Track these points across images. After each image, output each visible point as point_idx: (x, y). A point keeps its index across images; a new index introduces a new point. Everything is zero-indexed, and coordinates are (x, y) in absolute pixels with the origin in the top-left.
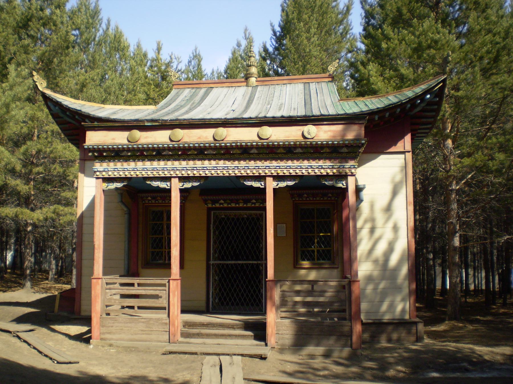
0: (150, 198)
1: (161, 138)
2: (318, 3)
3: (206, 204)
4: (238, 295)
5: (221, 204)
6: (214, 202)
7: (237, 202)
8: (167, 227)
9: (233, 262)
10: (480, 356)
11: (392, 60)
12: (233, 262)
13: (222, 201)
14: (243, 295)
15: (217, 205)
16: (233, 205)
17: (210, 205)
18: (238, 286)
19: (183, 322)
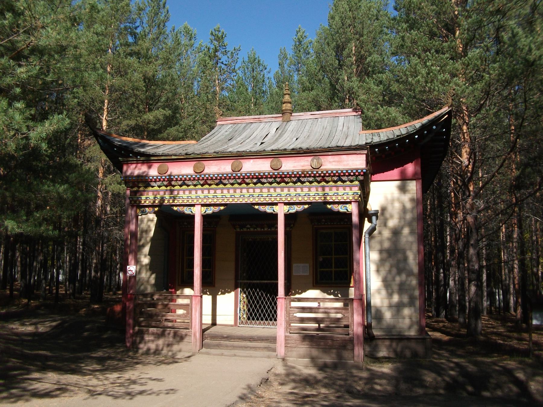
0: (185, 223)
1: (236, 343)
2: (363, 4)
3: (235, 228)
4: (262, 311)
5: (248, 228)
6: (242, 227)
7: (262, 227)
8: (15, 336)
9: (258, 282)
10: (400, 332)
11: (456, 56)
12: (258, 282)
13: (248, 226)
14: (267, 311)
15: (245, 230)
16: (259, 229)
17: (238, 230)
18: (262, 303)
19: (214, 286)
